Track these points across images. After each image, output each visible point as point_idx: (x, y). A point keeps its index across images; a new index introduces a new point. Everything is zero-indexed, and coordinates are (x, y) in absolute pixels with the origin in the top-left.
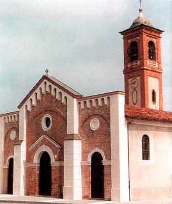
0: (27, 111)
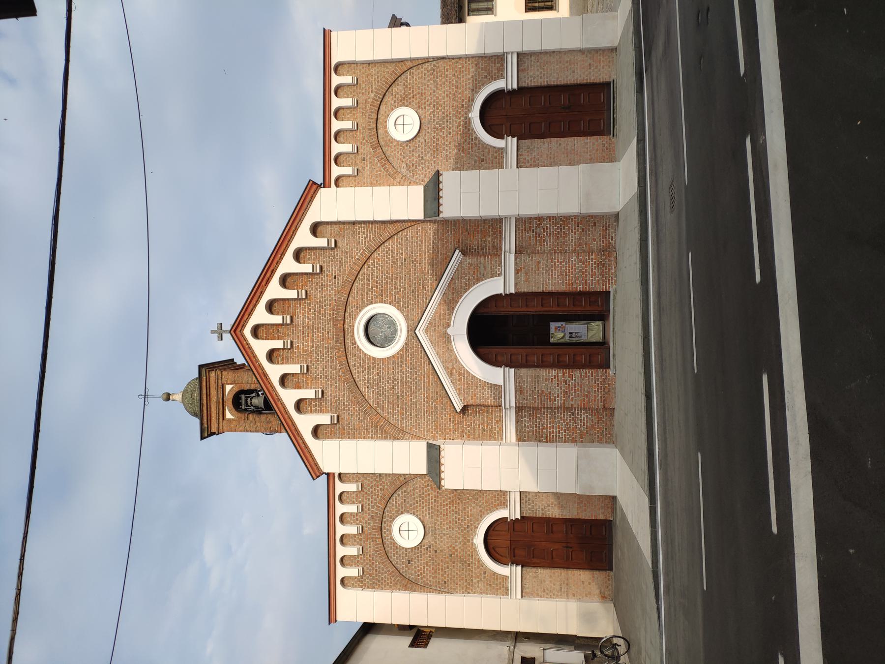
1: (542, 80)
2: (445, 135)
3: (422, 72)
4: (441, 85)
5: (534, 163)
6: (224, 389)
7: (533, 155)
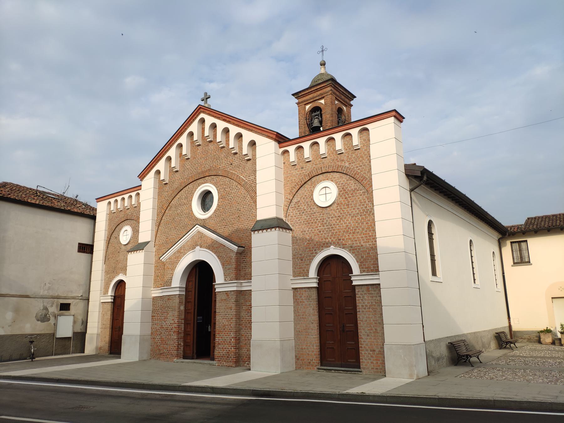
0: (171, 169)
1: (361, 306)
2: (319, 228)
3: (365, 202)
4: (355, 220)
5: (299, 302)
6: (322, 99)
7: (306, 301)
